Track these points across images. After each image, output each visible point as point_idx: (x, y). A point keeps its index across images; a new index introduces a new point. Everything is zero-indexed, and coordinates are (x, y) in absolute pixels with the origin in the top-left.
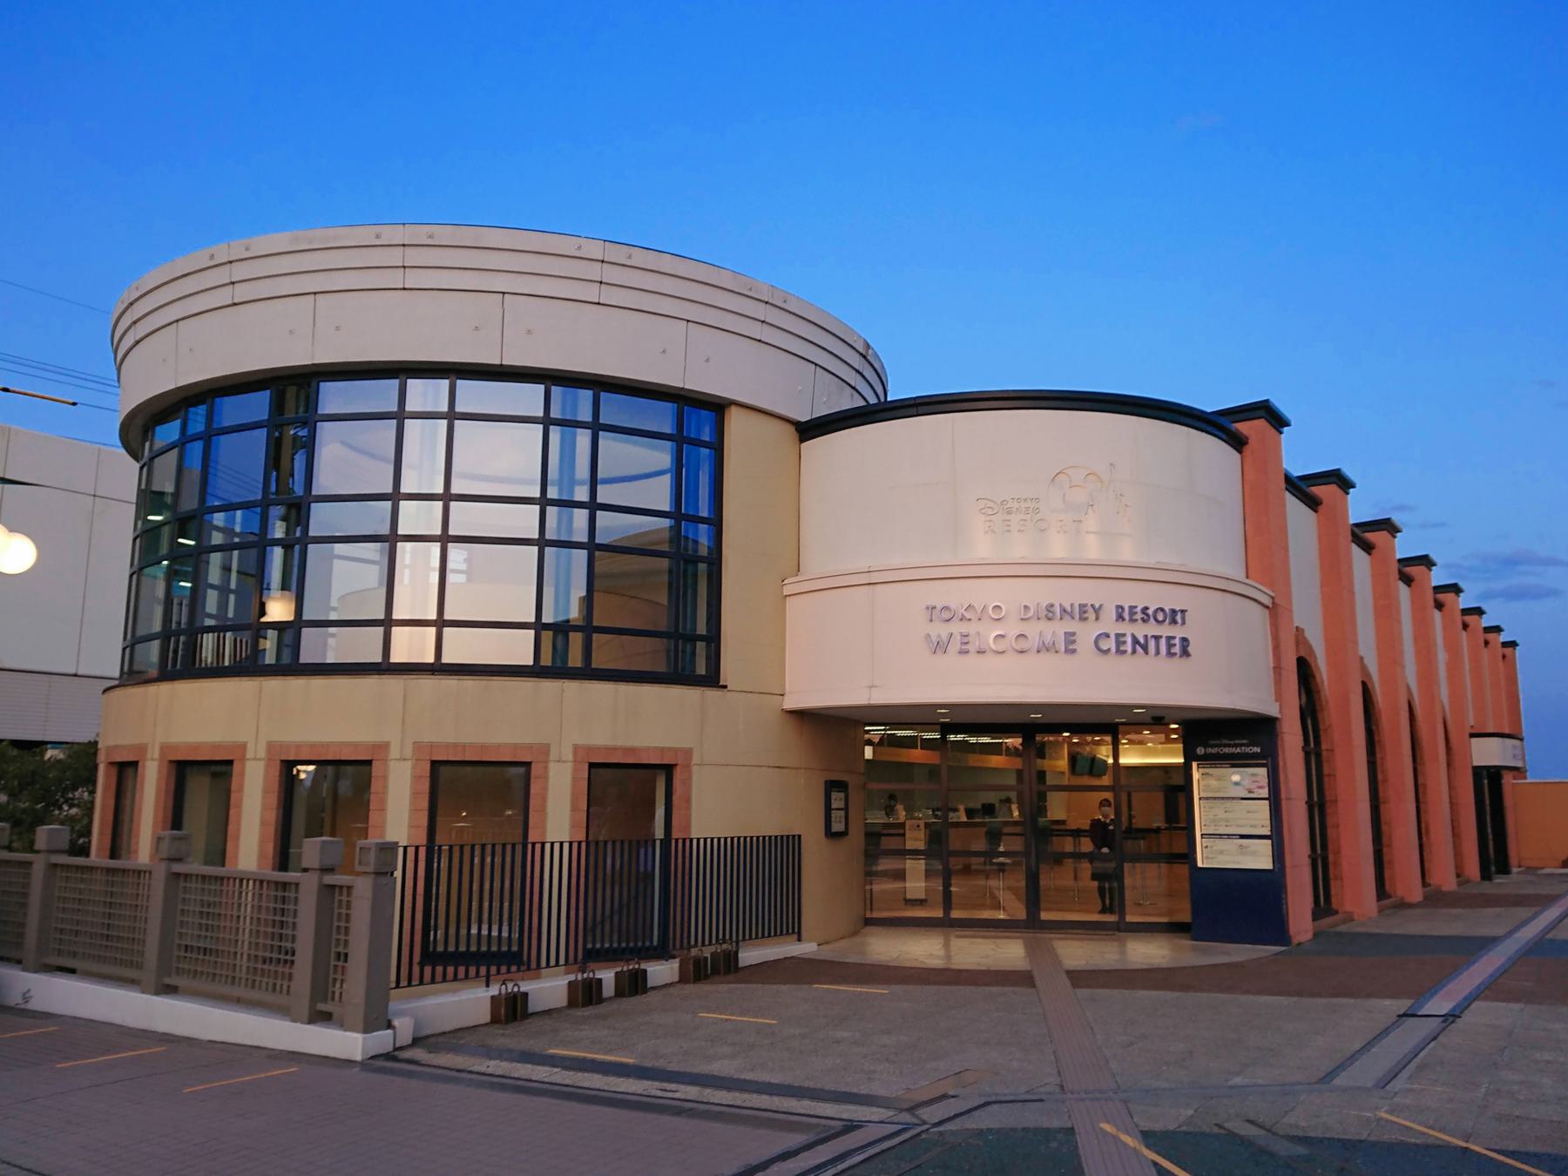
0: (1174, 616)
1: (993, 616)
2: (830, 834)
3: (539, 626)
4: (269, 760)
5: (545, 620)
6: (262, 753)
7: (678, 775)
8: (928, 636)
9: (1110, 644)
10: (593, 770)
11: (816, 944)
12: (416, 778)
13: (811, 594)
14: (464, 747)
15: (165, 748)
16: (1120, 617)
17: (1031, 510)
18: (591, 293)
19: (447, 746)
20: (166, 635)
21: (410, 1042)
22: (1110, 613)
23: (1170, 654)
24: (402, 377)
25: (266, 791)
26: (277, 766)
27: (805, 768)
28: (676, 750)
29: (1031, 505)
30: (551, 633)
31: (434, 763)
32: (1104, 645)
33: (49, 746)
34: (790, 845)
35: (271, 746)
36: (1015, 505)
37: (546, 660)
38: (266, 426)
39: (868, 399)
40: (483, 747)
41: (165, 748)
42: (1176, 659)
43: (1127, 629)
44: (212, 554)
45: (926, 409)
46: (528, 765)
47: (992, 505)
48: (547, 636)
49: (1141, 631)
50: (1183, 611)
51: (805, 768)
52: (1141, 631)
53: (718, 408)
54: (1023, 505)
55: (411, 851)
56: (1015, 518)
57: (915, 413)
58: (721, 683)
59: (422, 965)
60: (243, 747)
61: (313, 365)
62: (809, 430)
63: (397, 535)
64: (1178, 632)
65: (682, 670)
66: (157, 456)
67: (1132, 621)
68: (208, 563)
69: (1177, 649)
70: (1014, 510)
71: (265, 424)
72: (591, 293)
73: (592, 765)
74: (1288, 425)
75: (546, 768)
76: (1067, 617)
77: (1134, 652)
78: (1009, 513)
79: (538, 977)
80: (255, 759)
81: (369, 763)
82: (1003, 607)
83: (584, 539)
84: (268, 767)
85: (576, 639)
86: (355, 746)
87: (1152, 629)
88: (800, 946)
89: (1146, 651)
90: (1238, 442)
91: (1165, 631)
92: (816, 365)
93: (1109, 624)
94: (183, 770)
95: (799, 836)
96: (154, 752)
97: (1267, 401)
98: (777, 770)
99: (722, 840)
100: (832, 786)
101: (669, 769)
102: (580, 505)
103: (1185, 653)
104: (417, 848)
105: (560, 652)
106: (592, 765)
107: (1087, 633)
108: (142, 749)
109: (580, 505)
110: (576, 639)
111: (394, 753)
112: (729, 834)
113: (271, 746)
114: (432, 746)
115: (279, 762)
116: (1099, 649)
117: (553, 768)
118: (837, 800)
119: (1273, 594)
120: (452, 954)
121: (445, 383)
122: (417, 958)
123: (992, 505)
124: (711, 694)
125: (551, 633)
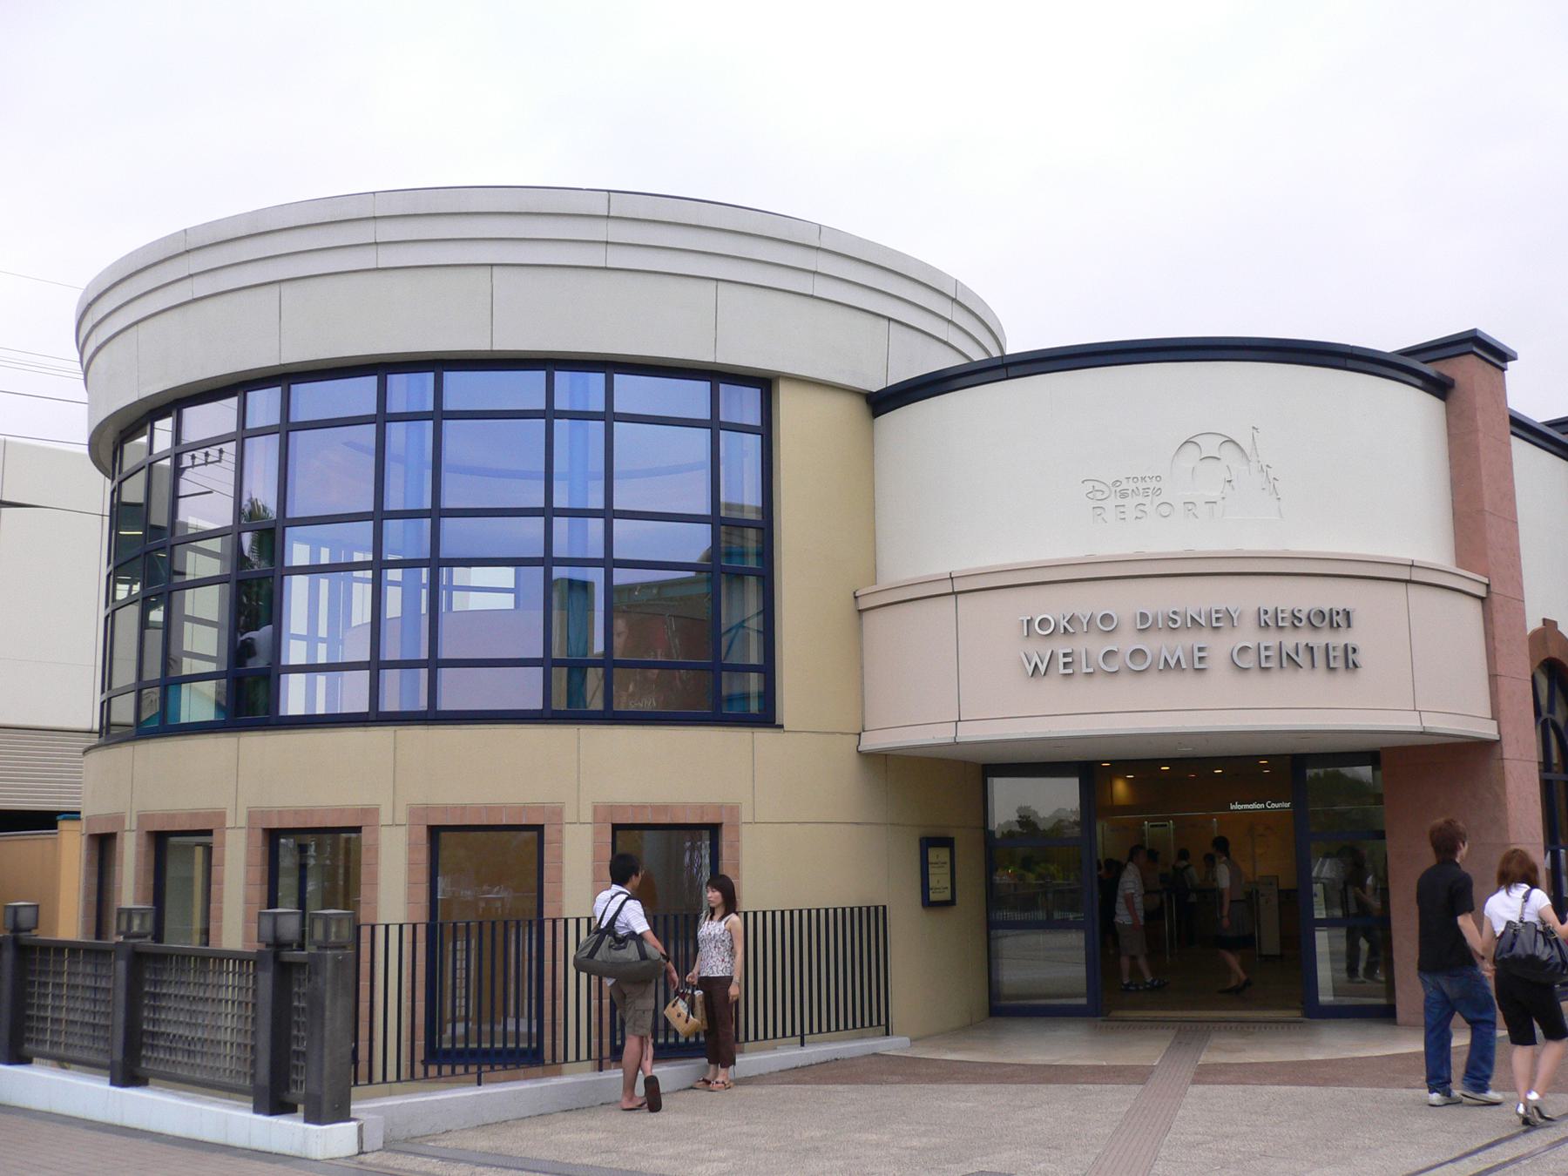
1: (1101, 627)
2: (927, 903)
3: (547, 663)
4: (250, 828)
5: (556, 654)
6: (243, 822)
9: (1248, 661)
10: (618, 833)
11: (907, 1039)
12: (412, 846)
13: (1343, 563)
15: (142, 818)
17: (1150, 491)
20: (140, 688)
21: (357, 1152)
22: (1249, 622)
24: (241, 394)
27: (891, 824)
28: (720, 807)
29: (1153, 484)
30: (565, 670)
31: (542, 826)
33: (62, 816)
36: (1131, 486)
37: (560, 703)
38: (234, 440)
39: (992, 353)
41: (142, 818)
42: (1342, 673)
43: (1271, 639)
44: (187, 591)
45: (984, 376)
46: (539, 829)
47: (1101, 487)
48: (560, 675)
49: (1290, 640)
51: (891, 824)
52: (1290, 640)
53: (765, 383)
54: (1141, 485)
55: (407, 931)
56: (1130, 502)
57: (1005, 377)
58: (777, 723)
59: (426, 1063)
60: (558, 812)
61: (281, 365)
62: (882, 402)
63: (712, 524)
64: (1339, 640)
66: (125, 479)
68: (757, 541)
69: (1340, 664)
70: (1129, 492)
71: (234, 438)
73: (616, 828)
74: (1514, 359)
75: (561, 831)
78: (1124, 495)
79: (559, 1073)
80: (130, 831)
81: (358, 830)
82: (1050, 618)
83: (600, 554)
84: (249, 836)
85: (594, 677)
87: (1305, 637)
88: (886, 1041)
90: (1440, 388)
91: (1319, 640)
92: (890, 319)
93: (1248, 636)
94: (160, 842)
95: (884, 907)
96: (131, 823)
97: (1475, 330)
98: (855, 826)
99: (840, 911)
100: (928, 843)
101: (714, 829)
104: (414, 926)
105: (576, 690)
106: (616, 828)
107: (1220, 647)
108: (119, 818)
110: (594, 677)
111: (385, 817)
112: (848, 904)
113: (251, 815)
114: (428, 809)
115: (260, 831)
117: (568, 830)
119: (1486, 581)
120: (692, 1045)
121: (430, 377)
122: (420, 1054)
123: (1101, 487)
124: (763, 736)
125: (565, 670)
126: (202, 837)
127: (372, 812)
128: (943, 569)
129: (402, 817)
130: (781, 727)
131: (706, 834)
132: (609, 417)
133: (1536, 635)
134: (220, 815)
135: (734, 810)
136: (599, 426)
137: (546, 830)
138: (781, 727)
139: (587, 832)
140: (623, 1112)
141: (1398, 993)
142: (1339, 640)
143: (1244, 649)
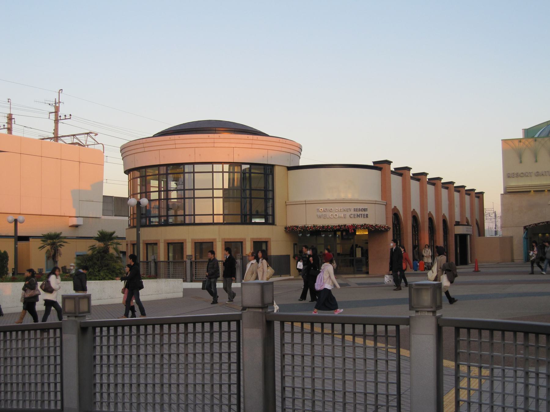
0: (365, 210)
4: (251, 241)
6: (190, 241)
7: (269, 243)
8: (317, 215)
9: (352, 216)
14: (230, 239)
16: (355, 211)
18: (250, 146)
19: (228, 239)
22: (352, 210)
23: (364, 217)
25: (192, 248)
26: (224, 243)
32: (352, 216)
34: (288, 256)
35: (192, 240)
40: (260, 239)
42: (365, 218)
43: (356, 213)
50: (367, 209)
52: (359, 213)
60: (186, 240)
64: (366, 213)
65: (244, 221)
67: (357, 211)
69: (365, 216)
72: (250, 146)
73: (225, 242)
76: (358, 217)
77: (357, 217)
85: (248, 217)
86: (210, 239)
87: (361, 213)
89: (360, 217)
91: (363, 213)
93: (353, 213)
102: (187, 173)
103: (367, 217)
106: (225, 242)
107: (348, 214)
109: (187, 173)
111: (218, 240)
113: (192, 240)
116: (426, 246)
117: (247, 242)
118: (296, 246)
124: (274, 226)
126: (241, 243)
127: (215, 239)
128: (304, 200)
129: (220, 240)
130: (276, 225)
131: (240, 243)
132: (213, 172)
133: (412, 212)
134: (245, 239)
135: (270, 239)
136: (192, 174)
137: (214, 243)
138: (276, 225)
139: (190, 244)
140: (395, 291)
141: (369, 268)
142: (366, 213)
143: (352, 214)
